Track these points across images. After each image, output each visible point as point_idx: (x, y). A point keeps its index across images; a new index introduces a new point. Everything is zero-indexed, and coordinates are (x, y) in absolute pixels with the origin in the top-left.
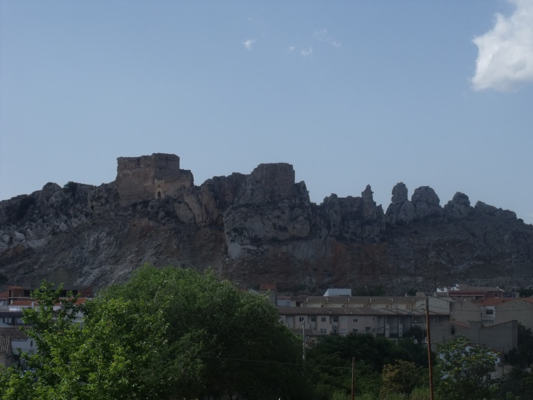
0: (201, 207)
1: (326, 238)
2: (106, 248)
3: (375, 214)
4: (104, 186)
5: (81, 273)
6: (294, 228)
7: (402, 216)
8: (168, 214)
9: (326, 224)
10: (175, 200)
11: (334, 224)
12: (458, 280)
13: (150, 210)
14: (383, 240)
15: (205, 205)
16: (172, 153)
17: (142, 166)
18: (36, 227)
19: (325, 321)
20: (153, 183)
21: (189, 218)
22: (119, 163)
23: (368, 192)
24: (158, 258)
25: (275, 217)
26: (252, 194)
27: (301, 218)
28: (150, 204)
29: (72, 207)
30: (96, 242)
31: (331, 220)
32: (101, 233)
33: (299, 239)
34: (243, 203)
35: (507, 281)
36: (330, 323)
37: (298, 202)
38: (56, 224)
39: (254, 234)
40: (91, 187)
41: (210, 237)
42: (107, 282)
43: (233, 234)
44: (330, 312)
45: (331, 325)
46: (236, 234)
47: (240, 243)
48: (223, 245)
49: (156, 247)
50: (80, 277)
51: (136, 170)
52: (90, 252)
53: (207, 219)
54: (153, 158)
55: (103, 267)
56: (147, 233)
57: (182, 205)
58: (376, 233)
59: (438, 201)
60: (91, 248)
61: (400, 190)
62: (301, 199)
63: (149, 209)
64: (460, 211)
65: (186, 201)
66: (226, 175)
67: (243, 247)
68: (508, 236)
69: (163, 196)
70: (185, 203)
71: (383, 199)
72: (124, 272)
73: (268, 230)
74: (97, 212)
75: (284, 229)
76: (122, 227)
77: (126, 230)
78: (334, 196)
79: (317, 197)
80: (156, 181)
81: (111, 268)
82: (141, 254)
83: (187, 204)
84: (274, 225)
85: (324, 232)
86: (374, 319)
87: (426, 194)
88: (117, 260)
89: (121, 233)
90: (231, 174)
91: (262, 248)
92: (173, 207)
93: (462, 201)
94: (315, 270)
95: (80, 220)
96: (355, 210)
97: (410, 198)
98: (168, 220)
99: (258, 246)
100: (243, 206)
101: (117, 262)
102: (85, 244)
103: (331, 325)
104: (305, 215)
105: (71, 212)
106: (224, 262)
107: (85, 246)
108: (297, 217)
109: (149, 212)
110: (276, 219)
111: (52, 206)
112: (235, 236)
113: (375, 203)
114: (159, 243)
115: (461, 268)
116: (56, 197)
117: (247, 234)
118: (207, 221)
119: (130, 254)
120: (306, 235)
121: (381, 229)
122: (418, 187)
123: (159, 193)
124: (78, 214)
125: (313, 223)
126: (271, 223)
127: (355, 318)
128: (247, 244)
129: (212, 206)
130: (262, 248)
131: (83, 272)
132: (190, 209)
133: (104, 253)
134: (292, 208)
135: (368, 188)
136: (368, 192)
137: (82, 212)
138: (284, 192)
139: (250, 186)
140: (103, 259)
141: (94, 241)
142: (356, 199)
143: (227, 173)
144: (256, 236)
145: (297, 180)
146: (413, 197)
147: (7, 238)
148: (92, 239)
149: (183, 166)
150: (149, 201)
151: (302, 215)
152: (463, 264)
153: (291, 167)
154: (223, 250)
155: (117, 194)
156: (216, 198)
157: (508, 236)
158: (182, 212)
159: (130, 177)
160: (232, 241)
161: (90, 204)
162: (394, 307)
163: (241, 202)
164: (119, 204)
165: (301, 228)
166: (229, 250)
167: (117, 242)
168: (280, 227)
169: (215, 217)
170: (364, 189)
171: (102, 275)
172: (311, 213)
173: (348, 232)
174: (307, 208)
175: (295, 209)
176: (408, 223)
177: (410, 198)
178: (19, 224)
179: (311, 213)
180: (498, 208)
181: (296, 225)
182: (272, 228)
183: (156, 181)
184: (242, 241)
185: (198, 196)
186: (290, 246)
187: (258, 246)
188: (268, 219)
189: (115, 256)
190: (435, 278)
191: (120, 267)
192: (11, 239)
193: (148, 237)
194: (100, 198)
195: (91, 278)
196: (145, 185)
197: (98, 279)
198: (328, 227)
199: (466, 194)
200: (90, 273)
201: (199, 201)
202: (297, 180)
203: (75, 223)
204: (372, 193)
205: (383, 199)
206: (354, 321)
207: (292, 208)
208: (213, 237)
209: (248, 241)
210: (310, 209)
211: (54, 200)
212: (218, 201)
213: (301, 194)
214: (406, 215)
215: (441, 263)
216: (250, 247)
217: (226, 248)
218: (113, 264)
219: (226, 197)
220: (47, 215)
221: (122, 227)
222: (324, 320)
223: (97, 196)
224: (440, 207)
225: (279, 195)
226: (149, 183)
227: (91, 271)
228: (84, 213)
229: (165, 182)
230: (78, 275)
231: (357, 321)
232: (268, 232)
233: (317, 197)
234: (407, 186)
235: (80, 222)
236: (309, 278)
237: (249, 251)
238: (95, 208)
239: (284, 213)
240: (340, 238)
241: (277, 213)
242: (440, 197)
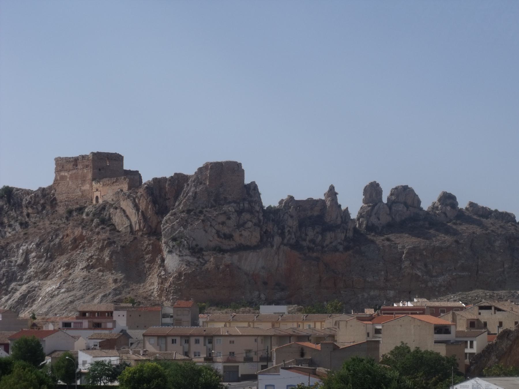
0: (138, 213)
1: (279, 247)
2: (36, 262)
3: (339, 219)
4: (43, 190)
5: (7, 291)
6: (241, 235)
7: (374, 220)
8: (103, 221)
9: (280, 231)
10: (111, 205)
11: (289, 231)
12: (437, 293)
13: (85, 217)
14: (347, 249)
15: (142, 212)
16: (114, 152)
17: (80, 166)
19: (199, 343)
20: (91, 186)
21: (126, 226)
22: (57, 164)
23: (332, 193)
24: (89, 272)
25: (219, 224)
27: (250, 224)
28: (86, 210)
30: (25, 254)
31: (286, 226)
32: (30, 244)
35: (486, 295)
36: (205, 345)
37: (246, 205)
39: (194, 243)
40: (28, 192)
41: (147, 247)
42: (34, 300)
43: (171, 244)
44: (205, 333)
45: (182, 347)
47: (178, 253)
48: (160, 256)
49: (88, 260)
50: (6, 295)
51: (74, 171)
52: (18, 265)
53: (144, 228)
54: (91, 158)
55: (32, 282)
56: (79, 243)
57: (118, 210)
58: (339, 241)
59: (419, 202)
60: (20, 261)
61: (373, 191)
62: (250, 203)
63: (84, 216)
64: (445, 213)
65: (122, 206)
66: (168, 176)
68: (500, 242)
69: (100, 201)
70: (121, 208)
71: (352, 203)
72: (52, 288)
73: (211, 239)
75: (229, 237)
76: (54, 236)
77: (57, 240)
78: (291, 198)
79: (270, 199)
80: (94, 183)
81: (39, 284)
82: (72, 268)
83: (124, 211)
84: (218, 232)
85: (277, 239)
86: (256, 340)
87: (405, 195)
88: (45, 274)
89: (52, 243)
90: (173, 175)
91: (203, 259)
92: (110, 215)
93: (448, 202)
94: (265, 283)
95: (14, 229)
96: (316, 214)
97: (385, 200)
98: (103, 228)
99: (198, 258)
101: (46, 278)
102: (14, 257)
103: (205, 347)
104: (255, 220)
106: (160, 276)
107: (13, 259)
108: (245, 223)
109: (83, 219)
110: (221, 226)
112: (173, 246)
113: (340, 206)
114: (90, 255)
115: (441, 279)
118: (145, 229)
119: (60, 268)
120: (255, 244)
121: (346, 236)
122: (394, 187)
123: (97, 197)
124: (12, 222)
125: (264, 230)
126: (214, 231)
127: (232, 339)
128: (186, 255)
129: (150, 213)
130: (203, 259)
131: (9, 289)
132: (127, 216)
133: (33, 267)
134: (240, 212)
135: (332, 188)
136: (332, 193)
138: (230, 195)
140: (32, 273)
141: (23, 254)
142: (317, 201)
143: (168, 174)
144: (197, 245)
145: (247, 181)
146: (388, 199)
148: (21, 251)
149: (127, 166)
150: (85, 207)
151: (251, 221)
152: (443, 275)
153: (239, 165)
154: (159, 261)
155: (55, 199)
156: (154, 202)
157: (500, 242)
158: (117, 219)
159: (68, 179)
160: (170, 252)
162: (306, 326)
164: (56, 211)
165: (250, 235)
166: (166, 262)
167: (47, 255)
168: (225, 235)
169: (154, 226)
170: (326, 190)
171: (29, 292)
172: (262, 218)
173: (305, 240)
174: (258, 212)
175: (243, 214)
176: (380, 228)
177: (385, 200)
179: (262, 218)
180: (493, 209)
182: (216, 237)
183: (94, 183)
184: (180, 251)
185: (135, 201)
186: (236, 257)
187: (198, 258)
188: (211, 226)
189: (44, 271)
190: (410, 292)
191: (49, 282)
193: (81, 249)
194: (36, 203)
195: (18, 295)
196: (83, 188)
197: (23, 297)
198: (282, 235)
199: (454, 193)
200: (16, 290)
201: (136, 206)
202: (247, 181)
203: (9, 233)
204: (336, 194)
205: (352, 203)
206: (230, 342)
207: (240, 212)
208: (151, 247)
210: (261, 215)
212: (157, 206)
213: (251, 197)
214: (379, 219)
215: (416, 274)
216: (189, 258)
217: (163, 260)
218: (42, 280)
221: (54, 236)
222: (197, 342)
224: (421, 209)
225: (225, 198)
226: (87, 187)
227: (18, 287)
228: (19, 221)
229: (103, 185)
230: (4, 292)
231: (233, 342)
232: (211, 241)
233: (270, 199)
234: (381, 186)
235: (13, 232)
236: (257, 293)
239: (229, 218)
240: (296, 246)
242: (421, 197)
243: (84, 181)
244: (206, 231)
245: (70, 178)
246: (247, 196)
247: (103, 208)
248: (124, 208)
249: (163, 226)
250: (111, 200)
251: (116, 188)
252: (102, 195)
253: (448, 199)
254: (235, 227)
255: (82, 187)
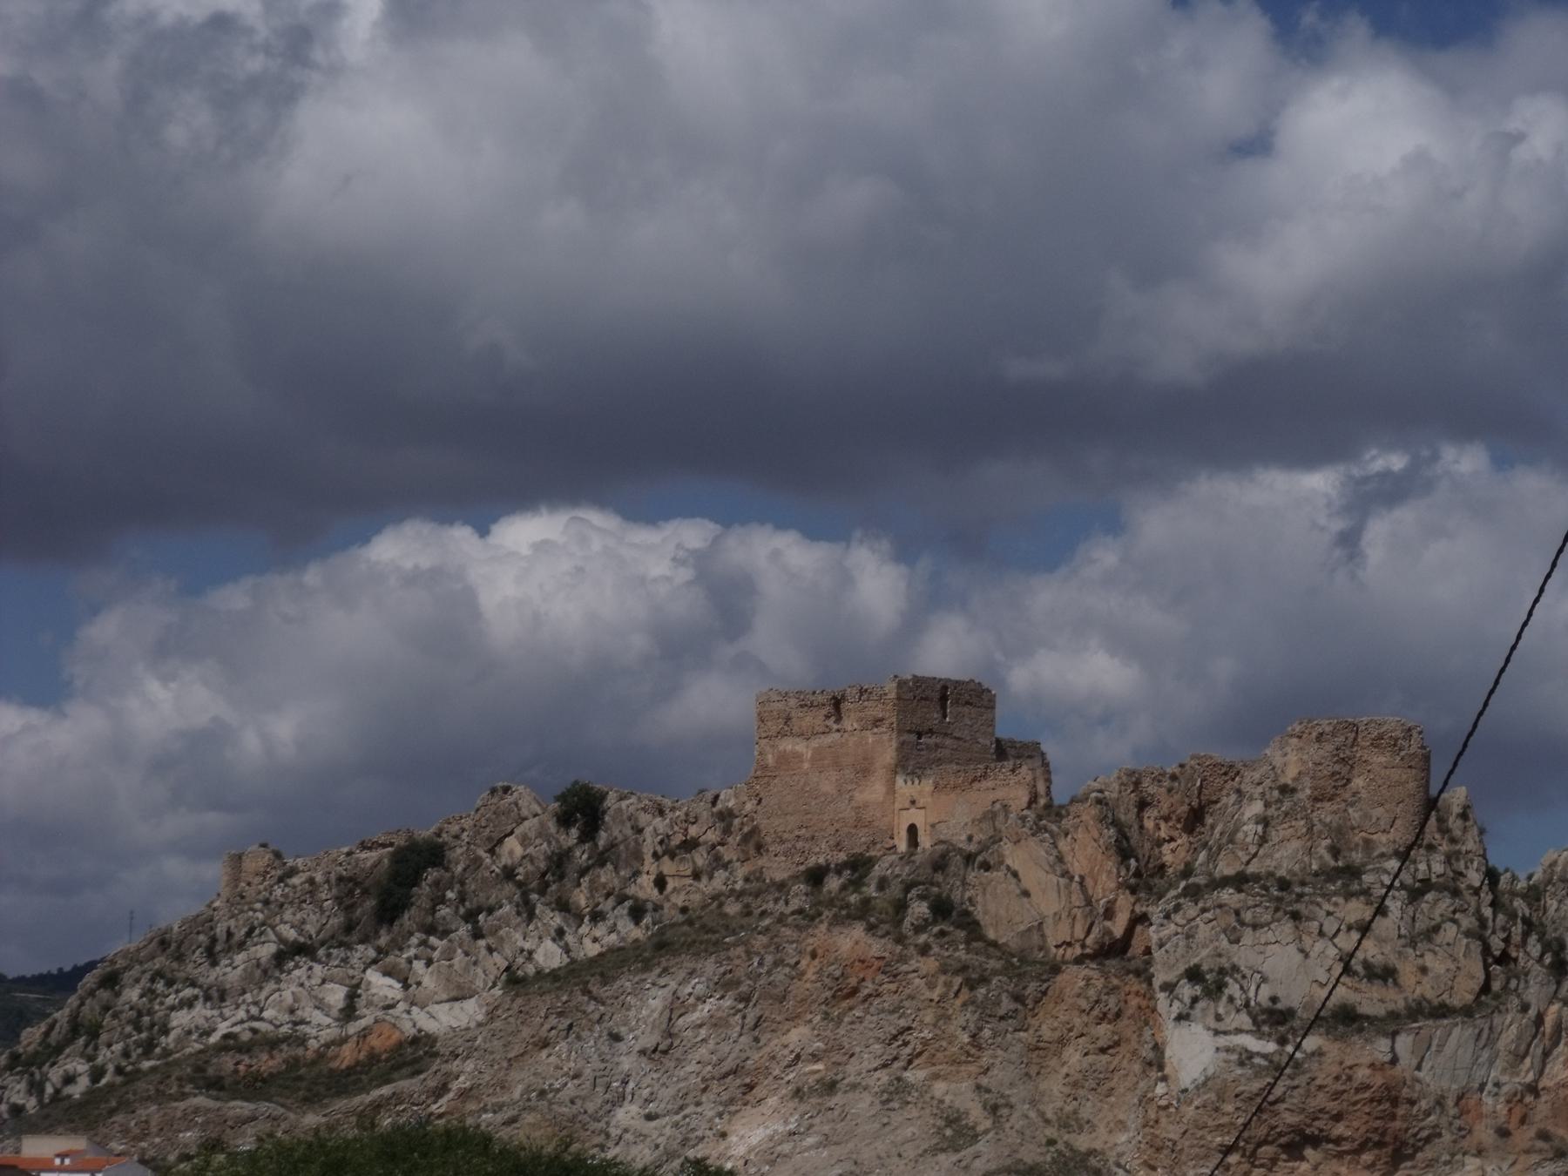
6: (1424, 970)
8: (942, 909)
17: (849, 723)
18: (449, 955)
20: (891, 789)
21: (1022, 928)
26: (1263, 840)
27: (1450, 931)
28: (877, 871)
29: (585, 881)
33: (1441, 1011)
34: (1229, 871)
37: (1438, 868)
38: (520, 943)
39: (1265, 992)
46: (1198, 990)
47: (1213, 1024)
63: (871, 890)
67: (1222, 1041)
69: (925, 841)
70: (1008, 868)
74: (679, 900)
75: (1385, 974)
80: (900, 781)
98: (942, 933)
99: (1282, 1041)
100: (1225, 882)
104: (1467, 922)
105: (581, 898)
111: (509, 873)
112: (1195, 1000)
116: (525, 841)
117: (1237, 993)
123: (912, 830)
128: (1238, 1031)
137: (621, 899)
139: (1257, 808)
147: (336, 996)
159: (806, 766)
161: (649, 865)
163: (1225, 868)
165: (1450, 968)
178: (383, 940)
181: (1429, 960)
183: (900, 781)
184: (1218, 1018)
192: (352, 997)
194: (690, 845)
196: (861, 797)
209: (1244, 1020)
211: (519, 851)
212: (1133, 862)
219: (1166, 848)
220: (490, 911)
223: (677, 840)
226: (874, 791)
237: (1246, 1057)
238: (671, 884)
241: (1357, 910)
243: (864, 771)
244: (1305, 954)
245: (813, 760)
246: (1437, 836)
247: (939, 864)
248: (1015, 866)
249: (1157, 932)
250: (964, 837)
251: (983, 796)
252: (932, 820)
253: (60, 970)
254: (1403, 941)
255: (856, 794)
